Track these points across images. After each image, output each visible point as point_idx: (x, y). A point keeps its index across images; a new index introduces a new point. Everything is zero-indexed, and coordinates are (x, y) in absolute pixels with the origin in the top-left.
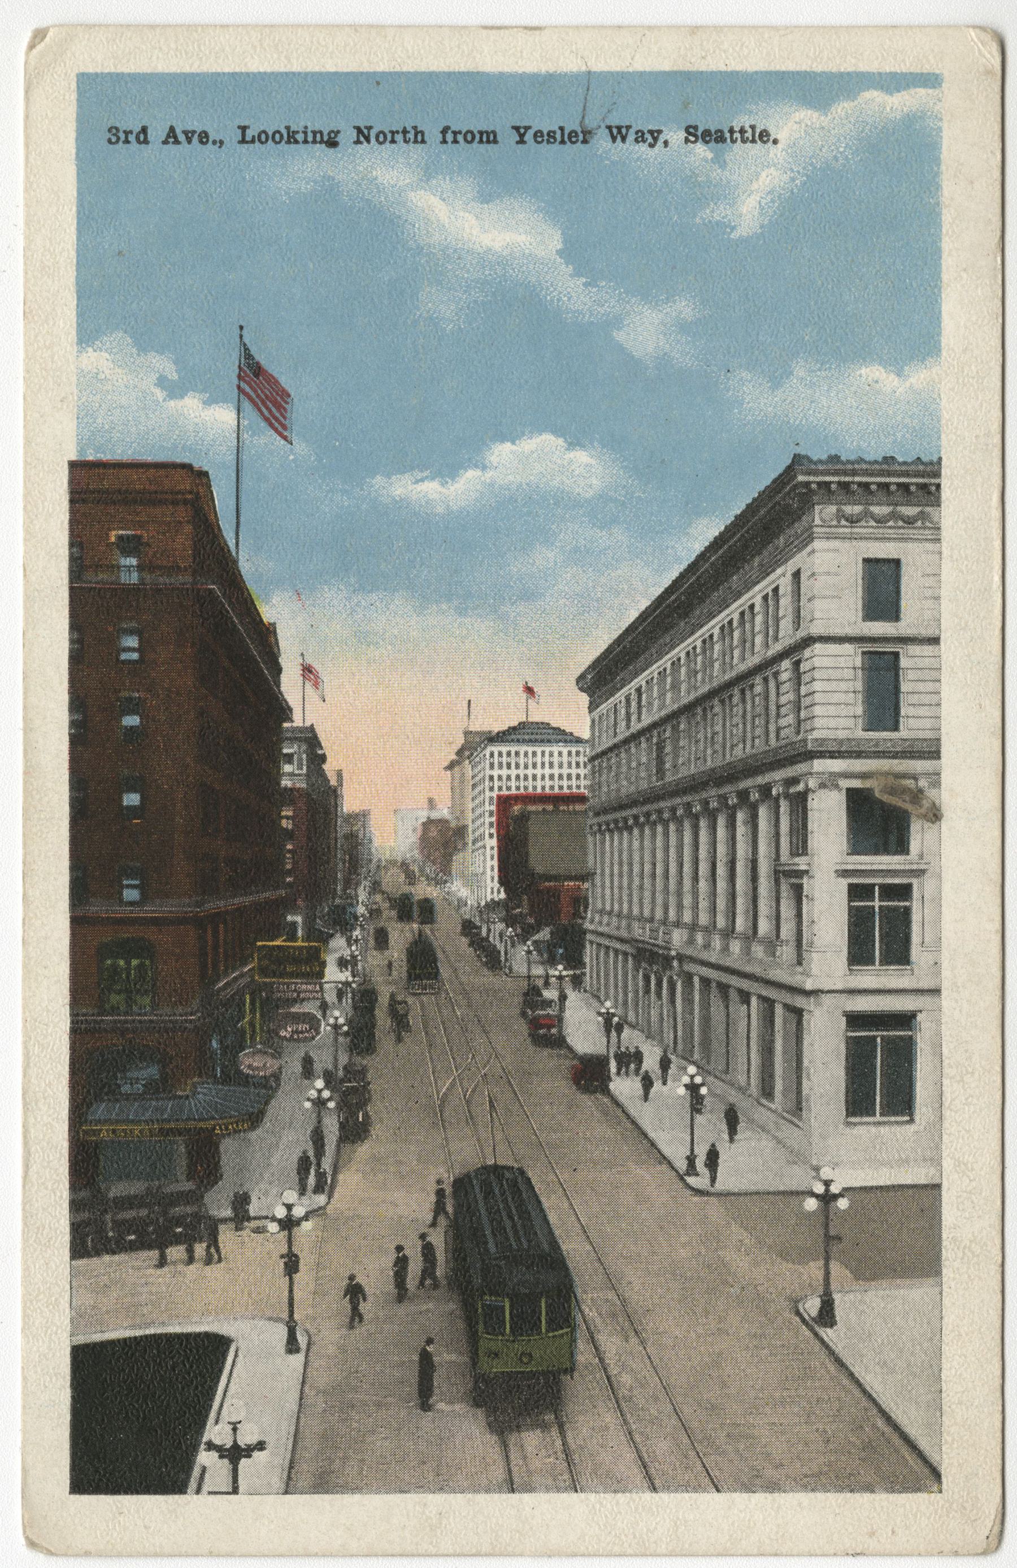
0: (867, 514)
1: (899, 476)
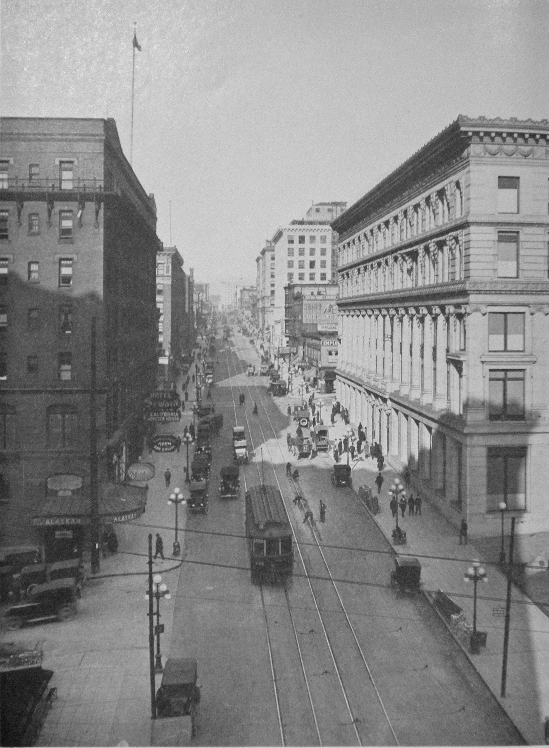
0: (500, 150)
1: (519, 128)
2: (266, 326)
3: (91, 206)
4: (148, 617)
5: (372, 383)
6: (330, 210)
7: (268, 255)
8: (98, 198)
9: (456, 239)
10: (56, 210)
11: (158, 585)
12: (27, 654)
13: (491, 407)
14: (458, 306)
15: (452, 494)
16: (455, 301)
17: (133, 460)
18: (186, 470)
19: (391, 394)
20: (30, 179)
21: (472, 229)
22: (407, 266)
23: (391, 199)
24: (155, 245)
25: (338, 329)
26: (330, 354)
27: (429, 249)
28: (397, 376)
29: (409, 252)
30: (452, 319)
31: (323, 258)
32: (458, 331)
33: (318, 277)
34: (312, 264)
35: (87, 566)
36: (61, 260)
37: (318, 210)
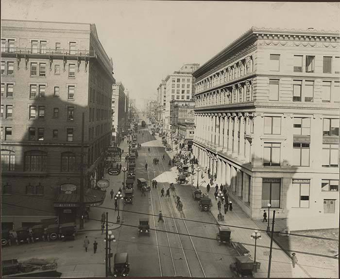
2: (161, 119)
3: (83, 63)
4: (105, 250)
5: (210, 147)
6: (191, 68)
7: (163, 87)
8: (87, 59)
9: (250, 82)
10: (30, 62)
11: (110, 235)
12: (50, 265)
13: (264, 160)
14: (250, 113)
15: (246, 199)
16: (249, 110)
17: (100, 178)
18: (123, 184)
19: (218, 152)
20: (56, 49)
21: (258, 78)
22: (227, 94)
23: (220, 63)
24: (113, 81)
25: (195, 122)
26: (191, 133)
27: (238, 86)
28: (221, 143)
29: (228, 88)
30: (247, 119)
31: (188, 89)
32: (250, 124)
33: (180, 98)
34: (183, 92)
35: (78, 226)
36: (31, 85)
37: (186, 67)
